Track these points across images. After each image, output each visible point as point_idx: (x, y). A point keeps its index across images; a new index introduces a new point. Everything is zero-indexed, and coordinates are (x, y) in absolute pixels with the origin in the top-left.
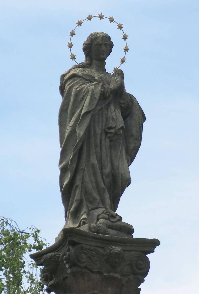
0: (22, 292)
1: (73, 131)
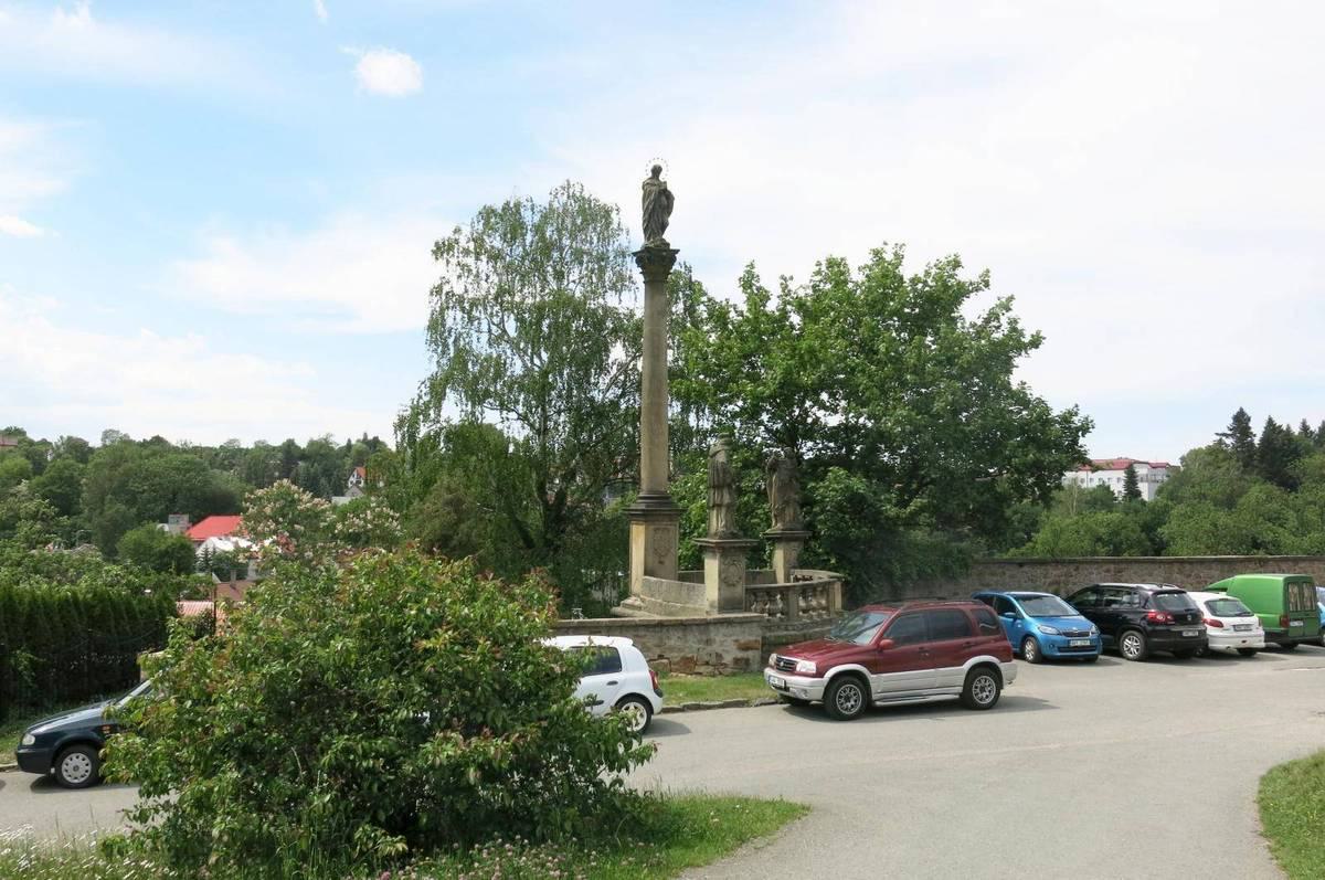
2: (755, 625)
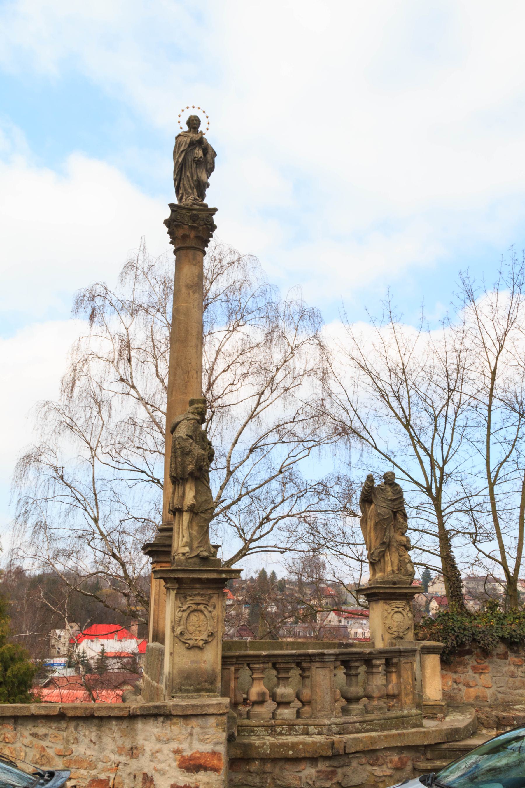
0: (249, 746)
1: (178, 161)
2: (212, 721)
